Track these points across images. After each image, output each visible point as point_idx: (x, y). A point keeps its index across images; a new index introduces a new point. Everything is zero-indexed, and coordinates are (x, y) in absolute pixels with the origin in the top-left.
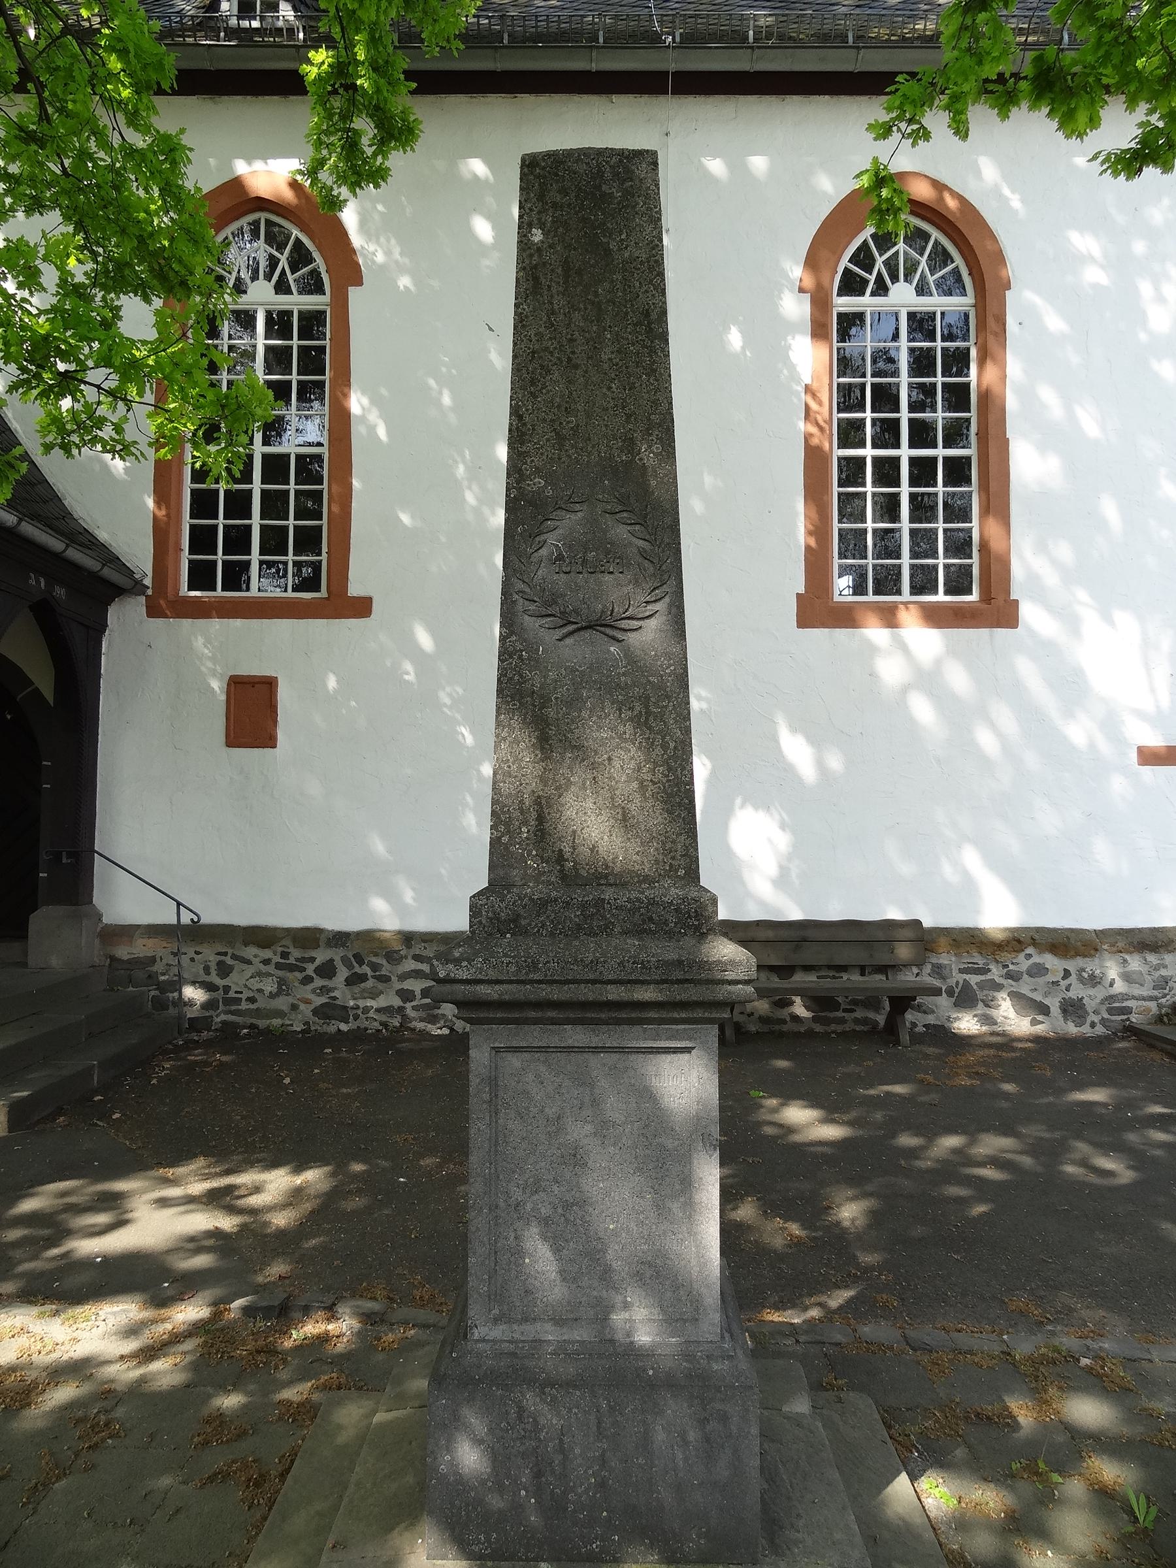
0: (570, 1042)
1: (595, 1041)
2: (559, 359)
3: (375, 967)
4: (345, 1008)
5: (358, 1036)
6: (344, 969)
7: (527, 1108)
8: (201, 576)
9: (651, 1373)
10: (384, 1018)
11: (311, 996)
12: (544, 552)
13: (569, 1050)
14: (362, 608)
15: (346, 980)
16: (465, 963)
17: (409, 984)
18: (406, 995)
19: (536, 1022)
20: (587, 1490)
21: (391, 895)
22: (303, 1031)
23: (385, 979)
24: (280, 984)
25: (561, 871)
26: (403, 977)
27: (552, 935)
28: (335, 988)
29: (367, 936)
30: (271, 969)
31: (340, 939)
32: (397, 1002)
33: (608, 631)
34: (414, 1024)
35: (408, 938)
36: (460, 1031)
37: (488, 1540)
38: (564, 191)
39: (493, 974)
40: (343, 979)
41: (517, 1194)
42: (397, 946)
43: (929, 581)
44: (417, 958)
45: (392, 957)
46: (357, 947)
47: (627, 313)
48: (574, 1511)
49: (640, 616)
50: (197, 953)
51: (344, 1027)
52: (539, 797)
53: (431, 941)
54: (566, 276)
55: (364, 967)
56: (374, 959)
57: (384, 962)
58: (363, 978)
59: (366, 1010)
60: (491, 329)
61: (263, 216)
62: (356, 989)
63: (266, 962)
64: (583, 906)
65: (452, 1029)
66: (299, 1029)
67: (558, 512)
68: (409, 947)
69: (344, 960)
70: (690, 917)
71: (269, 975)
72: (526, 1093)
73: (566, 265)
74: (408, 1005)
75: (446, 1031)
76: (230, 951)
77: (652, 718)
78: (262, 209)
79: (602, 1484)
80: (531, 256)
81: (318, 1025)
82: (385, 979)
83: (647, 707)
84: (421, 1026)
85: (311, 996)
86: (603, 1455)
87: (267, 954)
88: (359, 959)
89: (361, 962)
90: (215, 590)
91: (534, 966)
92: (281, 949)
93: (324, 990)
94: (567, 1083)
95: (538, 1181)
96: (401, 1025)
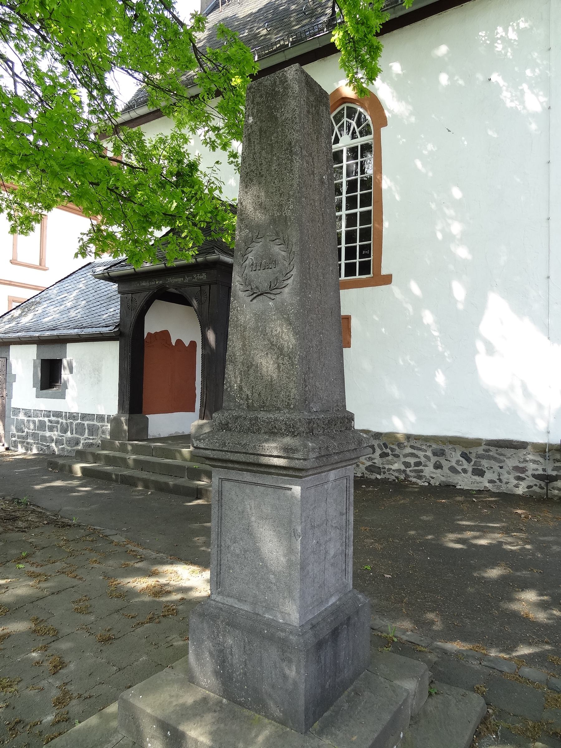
0: (245, 480)
1: (254, 480)
2: (256, 174)
3: (392, 450)
4: (380, 468)
5: (385, 481)
6: (379, 450)
7: (232, 506)
9: (266, 632)
10: (397, 474)
11: (365, 461)
12: (247, 262)
14: (387, 280)
15: (380, 455)
16: (202, 441)
17: (408, 460)
18: (407, 465)
19: (233, 469)
20: (240, 674)
21: (401, 416)
22: (361, 477)
23: (397, 456)
25: (247, 404)
26: (406, 456)
27: (240, 432)
28: (375, 459)
29: (391, 436)
31: (377, 436)
32: (403, 468)
33: (269, 295)
34: (410, 479)
35: (408, 437)
36: (433, 485)
37: (207, 681)
38: (261, 96)
39: (211, 447)
40: (378, 454)
41: (229, 542)
42: (402, 440)
44: (412, 447)
45: (400, 445)
46: (384, 440)
47: (282, 146)
48: (235, 682)
51: (379, 477)
52: (241, 371)
53: (419, 439)
54: (261, 135)
55: (388, 449)
56: (392, 446)
57: (397, 448)
58: (387, 455)
59: (389, 470)
60: (449, 131)
61: (345, 106)
62: (384, 459)
64: (251, 420)
65: (429, 483)
66: (359, 476)
67: (253, 244)
68: (408, 441)
69: (379, 446)
70: (290, 427)
72: (232, 499)
73: (261, 130)
74: (408, 469)
75: (427, 484)
77: (284, 334)
78: (345, 103)
79: (245, 674)
80: (248, 129)
81: (368, 475)
82: (397, 456)
83: (282, 329)
84: (414, 480)
85: (365, 461)
86: (245, 661)
88: (386, 446)
89: (386, 447)
91: (224, 444)
93: (370, 459)
95: (235, 538)
96: (405, 479)
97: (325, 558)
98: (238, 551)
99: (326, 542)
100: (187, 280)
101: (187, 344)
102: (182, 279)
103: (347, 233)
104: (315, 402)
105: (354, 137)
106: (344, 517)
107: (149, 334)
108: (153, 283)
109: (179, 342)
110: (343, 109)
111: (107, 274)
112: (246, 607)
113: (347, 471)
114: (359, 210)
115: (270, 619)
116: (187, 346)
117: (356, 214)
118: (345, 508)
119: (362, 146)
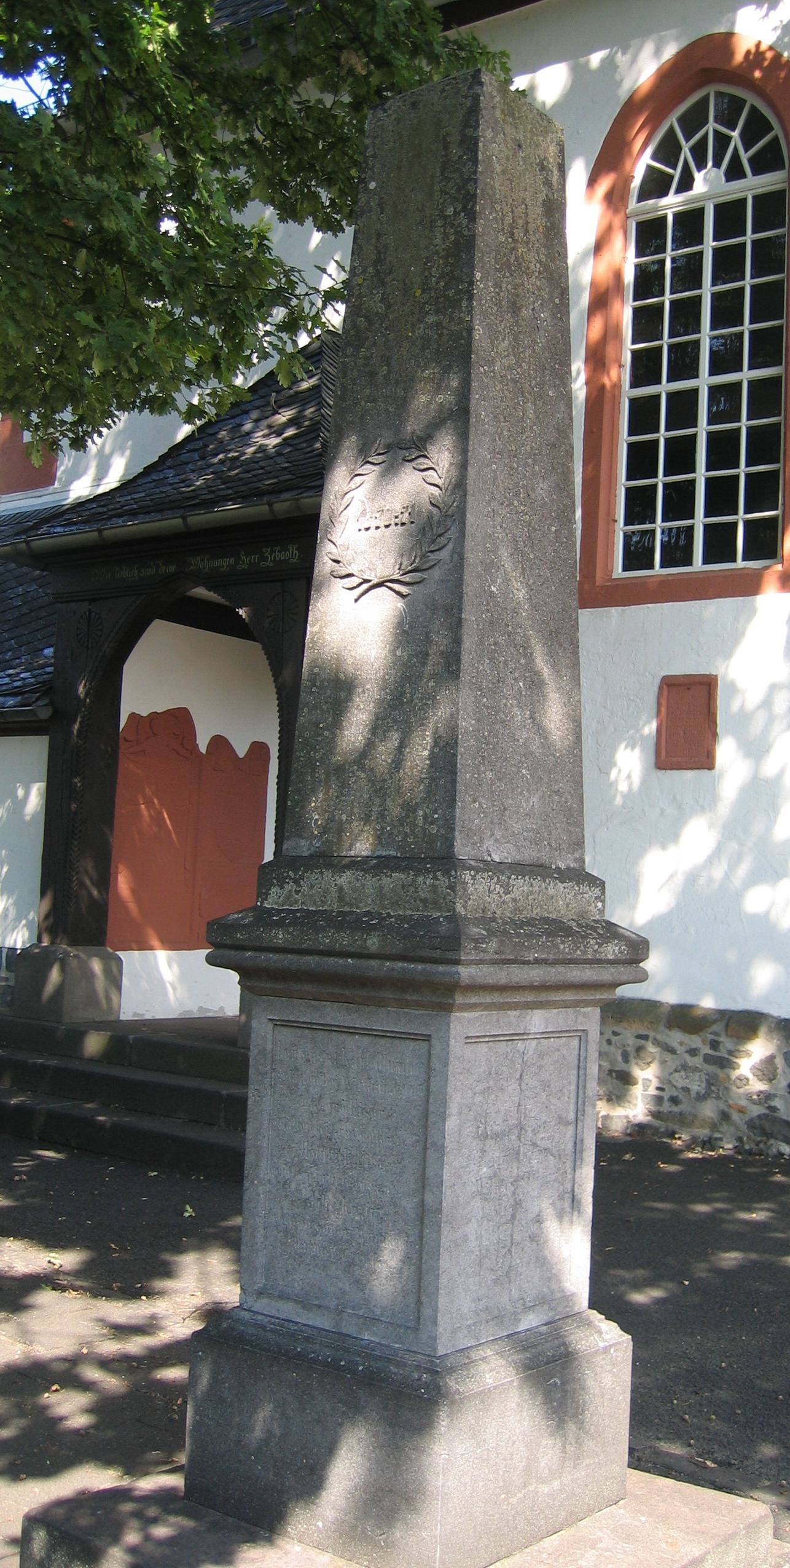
0: (328, 1021)
7: (296, 1085)
8: (637, 555)
13: (329, 1029)
24: (709, 1084)
30: (698, 1061)
43: (567, 501)
49: (425, 567)
50: (615, 1034)
61: (711, 90)
63: (693, 1052)
71: (696, 1069)
76: (651, 1034)
87: (695, 1041)
90: (651, 566)
92: (711, 1037)
94: (329, 1063)
97: (513, 1217)
98: (306, 1193)
99: (518, 1178)
100: (246, 561)
101: (241, 752)
102: (232, 561)
103: (713, 439)
104: (497, 840)
105: (735, 172)
106: (570, 1130)
107: (133, 716)
108: (151, 571)
109: (219, 743)
110: (705, 100)
111: (24, 546)
112: (322, 1321)
113: (580, 1018)
114: (745, 375)
115: (372, 1342)
116: (241, 755)
117: (738, 385)
118: (572, 1107)
119: (756, 198)
